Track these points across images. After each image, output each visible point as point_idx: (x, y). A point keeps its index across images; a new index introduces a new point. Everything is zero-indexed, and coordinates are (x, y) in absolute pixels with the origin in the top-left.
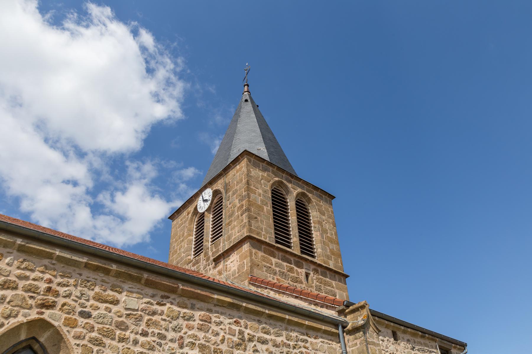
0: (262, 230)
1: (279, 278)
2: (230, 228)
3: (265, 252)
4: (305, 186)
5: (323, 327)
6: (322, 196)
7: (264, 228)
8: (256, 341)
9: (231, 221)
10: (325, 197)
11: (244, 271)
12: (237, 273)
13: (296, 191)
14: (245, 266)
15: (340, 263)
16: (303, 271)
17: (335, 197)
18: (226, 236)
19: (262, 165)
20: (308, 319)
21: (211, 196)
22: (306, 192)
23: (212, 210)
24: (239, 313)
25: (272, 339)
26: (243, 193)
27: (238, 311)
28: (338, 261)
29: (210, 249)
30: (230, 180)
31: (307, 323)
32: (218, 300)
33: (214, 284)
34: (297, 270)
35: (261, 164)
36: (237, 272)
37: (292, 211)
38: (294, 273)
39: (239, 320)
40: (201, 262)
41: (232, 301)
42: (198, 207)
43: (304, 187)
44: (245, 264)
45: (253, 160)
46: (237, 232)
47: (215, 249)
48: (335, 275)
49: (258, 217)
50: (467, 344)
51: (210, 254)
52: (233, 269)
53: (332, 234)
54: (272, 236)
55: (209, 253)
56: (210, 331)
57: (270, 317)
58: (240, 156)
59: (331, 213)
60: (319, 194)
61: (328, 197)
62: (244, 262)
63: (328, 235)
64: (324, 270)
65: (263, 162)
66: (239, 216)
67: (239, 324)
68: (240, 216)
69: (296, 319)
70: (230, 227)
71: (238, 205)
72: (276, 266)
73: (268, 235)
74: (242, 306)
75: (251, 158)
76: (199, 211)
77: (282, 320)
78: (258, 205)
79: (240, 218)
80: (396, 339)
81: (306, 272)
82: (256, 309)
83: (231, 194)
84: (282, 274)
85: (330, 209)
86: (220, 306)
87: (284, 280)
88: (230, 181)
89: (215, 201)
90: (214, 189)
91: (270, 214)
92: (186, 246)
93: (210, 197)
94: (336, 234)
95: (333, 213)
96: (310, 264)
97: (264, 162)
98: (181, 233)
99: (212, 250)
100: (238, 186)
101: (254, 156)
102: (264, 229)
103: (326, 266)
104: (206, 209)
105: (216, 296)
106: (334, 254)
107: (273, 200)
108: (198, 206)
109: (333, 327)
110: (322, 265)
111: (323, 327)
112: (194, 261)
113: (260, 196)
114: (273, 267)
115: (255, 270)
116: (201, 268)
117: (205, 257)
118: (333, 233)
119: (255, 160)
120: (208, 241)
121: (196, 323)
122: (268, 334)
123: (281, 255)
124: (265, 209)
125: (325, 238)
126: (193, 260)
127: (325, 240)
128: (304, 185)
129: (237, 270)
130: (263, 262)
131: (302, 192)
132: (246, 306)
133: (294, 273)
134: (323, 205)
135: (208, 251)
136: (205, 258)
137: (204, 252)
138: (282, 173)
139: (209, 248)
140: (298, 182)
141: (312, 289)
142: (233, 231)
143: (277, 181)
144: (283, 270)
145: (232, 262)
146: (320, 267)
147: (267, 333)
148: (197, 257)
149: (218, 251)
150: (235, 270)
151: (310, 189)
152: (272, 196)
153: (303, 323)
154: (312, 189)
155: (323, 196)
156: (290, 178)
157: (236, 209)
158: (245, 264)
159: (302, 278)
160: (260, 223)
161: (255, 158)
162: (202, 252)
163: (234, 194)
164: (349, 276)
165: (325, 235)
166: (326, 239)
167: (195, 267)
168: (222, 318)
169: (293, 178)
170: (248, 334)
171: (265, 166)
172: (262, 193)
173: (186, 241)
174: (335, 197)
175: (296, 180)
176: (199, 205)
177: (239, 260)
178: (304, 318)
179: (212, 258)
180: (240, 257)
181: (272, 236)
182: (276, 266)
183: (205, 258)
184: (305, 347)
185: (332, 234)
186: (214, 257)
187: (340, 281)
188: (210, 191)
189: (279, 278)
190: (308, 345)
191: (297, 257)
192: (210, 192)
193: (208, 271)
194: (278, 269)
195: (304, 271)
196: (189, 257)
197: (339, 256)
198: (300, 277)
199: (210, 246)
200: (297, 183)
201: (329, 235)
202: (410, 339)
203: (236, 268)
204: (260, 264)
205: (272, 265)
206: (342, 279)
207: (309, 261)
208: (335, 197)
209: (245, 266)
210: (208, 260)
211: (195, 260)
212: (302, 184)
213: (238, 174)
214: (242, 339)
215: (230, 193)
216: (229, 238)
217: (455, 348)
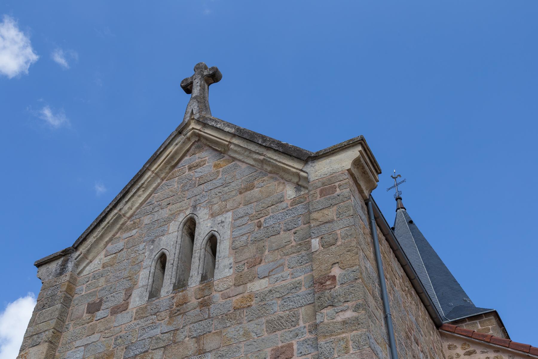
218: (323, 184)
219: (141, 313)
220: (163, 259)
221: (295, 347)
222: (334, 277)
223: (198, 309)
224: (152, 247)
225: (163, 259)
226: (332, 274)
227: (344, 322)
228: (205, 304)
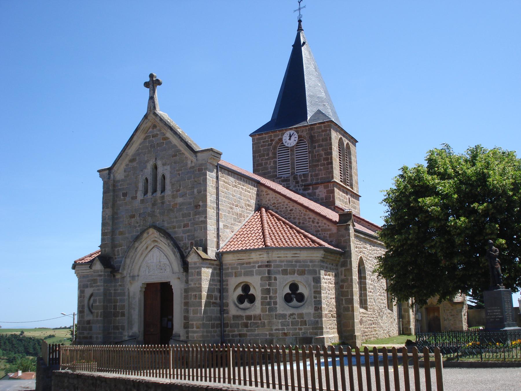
14: (332, 198)
17: (358, 142)
30: (316, 135)
65: (336, 126)
70: (317, 168)
90: (299, 134)
142: (320, 172)
149: (306, 180)
203: (324, 196)
209: (332, 198)
218: (199, 166)
219: (142, 201)
220: (147, 179)
221: (189, 224)
222: (200, 205)
223: (161, 204)
224: (142, 173)
225: (147, 179)
226: (199, 204)
227: (201, 221)
228: (163, 203)
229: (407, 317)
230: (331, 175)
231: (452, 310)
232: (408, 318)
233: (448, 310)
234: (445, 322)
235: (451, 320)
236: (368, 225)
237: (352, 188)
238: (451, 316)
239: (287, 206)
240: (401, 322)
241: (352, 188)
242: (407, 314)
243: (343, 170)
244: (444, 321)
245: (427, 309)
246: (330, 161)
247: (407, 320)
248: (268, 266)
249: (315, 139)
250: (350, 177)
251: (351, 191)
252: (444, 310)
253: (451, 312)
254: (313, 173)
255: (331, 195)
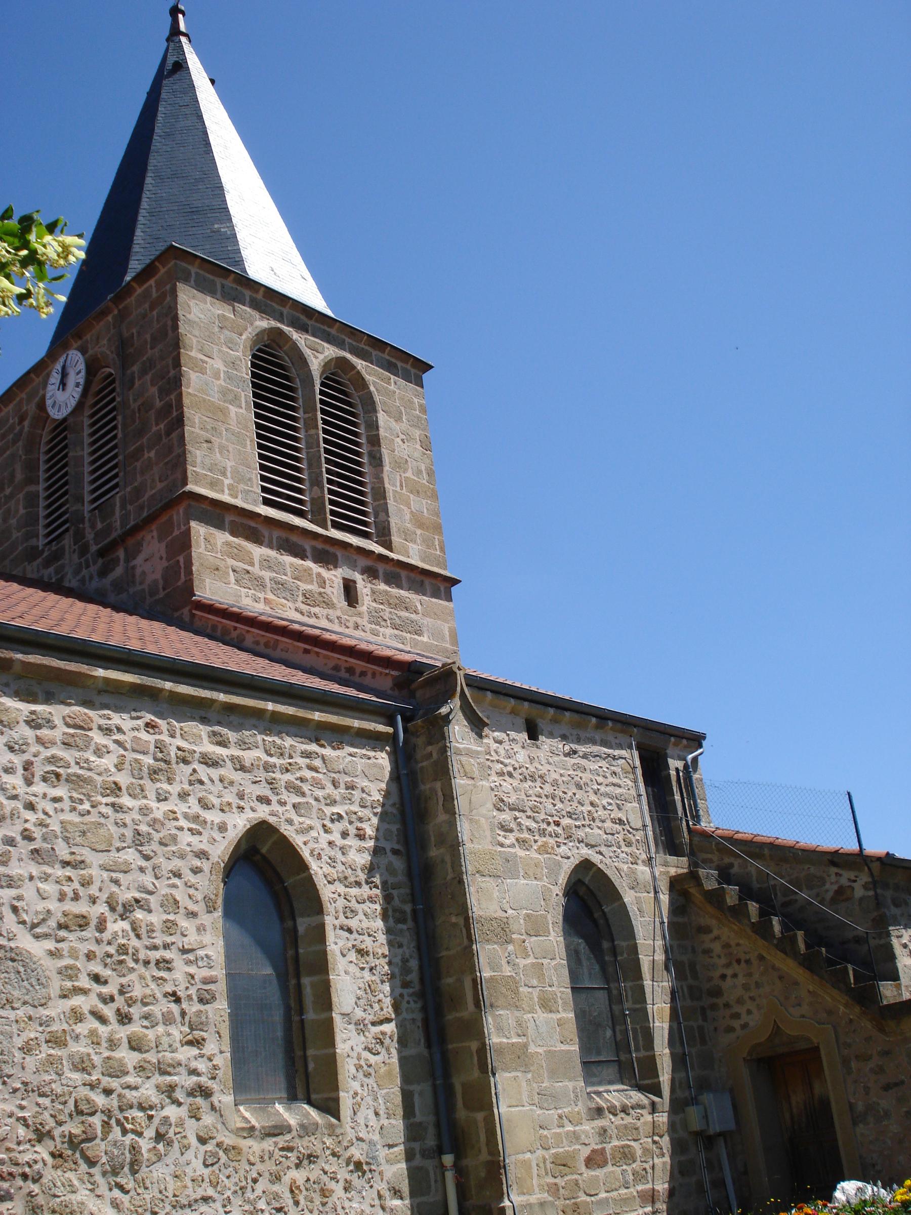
0: (224, 474)
1: (271, 596)
2: (138, 468)
3: (233, 534)
4: (347, 340)
5: (356, 724)
6: (395, 366)
7: (231, 467)
8: (196, 762)
9: (140, 450)
10: (405, 365)
11: (179, 583)
12: (161, 590)
13: (321, 357)
15: (437, 547)
16: (335, 576)
17: (432, 367)
18: (128, 489)
19: (223, 286)
20: (320, 707)
21: (83, 373)
22: (348, 356)
23: (88, 412)
24: (157, 706)
25: (233, 756)
26: (169, 372)
27: (154, 701)
28: (433, 544)
29: (87, 524)
30: (134, 331)
31: (317, 716)
32: (107, 680)
33: (95, 646)
34: (319, 575)
35: (218, 281)
36: (161, 587)
37: (310, 415)
38: (313, 581)
39: (156, 720)
40: (67, 556)
41: (139, 682)
42: (49, 402)
43: (344, 341)
44: (182, 566)
45: (197, 274)
46: (157, 479)
47: (102, 522)
48: (422, 582)
49: (213, 439)
50: (707, 736)
51: (90, 535)
52: (149, 579)
53: (419, 472)
54: (251, 489)
55: (87, 535)
56: (92, 747)
57: (230, 708)
58: (159, 262)
59: (418, 412)
60: (387, 360)
61: (413, 366)
62: (178, 561)
63: (406, 475)
64: (393, 569)
65: (226, 277)
66: (161, 435)
67: (157, 730)
68: (164, 437)
69: (290, 710)
71: (158, 404)
72: (262, 567)
73: (242, 486)
74: (161, 690)
75: (190, 267)
76: (51, 413)
77: (259, 714)
78: (213, 403)
79: (164, 440)
80: (533, 735)
81: (344, 579)
82: (196, 694)
83: (136, 372)
84: (279, 587)
85: (416, 400)
86: (113, 693)
87: (286, 602)
88: (133, 334)
89: (95, 388)
91: (246, 428)
92: (22, 511)
93: (80, 375)
94: (430, 473)
95: (423, 409)
96: (355, 557)
97: (228, 276)
98: (5, 474)
99: (93, 526)
100: (156, 350)
101: (198, 261)
102: (229, 469)
103: (398, 561)
104: (70, 409)
105: (100, 672)
106: (424, 524)
107: (254, 385)
108: (47, 401)
109: (382, 720)
110: (388, 557)
111: (356, 724)
112: (46, 554)
113: (218, 379)
114: (256, 570)
115: (207, 580)
116: (67, 573)
117: (74, 545)
118: (423, 468)
119: (202, 272)
120: (80, 499)
121: (60, 731)
122: (225, 746)
123: (277, 538)
124: (233, 415)
125: (398, 484)
126: (43, 551)
127: (398, 489)
128: (344, 337)
129: (161, 583)
130: (228, 559)
131: (337, 358)
132: (173, 690)
133: (311, 582)
134: (398, 391)
135: (84, 528)
136: (76, 547)
137: (71, 532)
138: (281, 306)
139: (87, 519)
140: (326, 328)
141: (359, 620)
143: (265, 330)
144: (284, 577)
145: (147, 559)
146: (382, 562)
147: (223, 744)
148: (54, 543)
149: (108, 529)
150: (155, 582)
151: (362, 346)
152: (254, 375)
153: (310, 716)
154: (367, 348)
155: (399, 364)
156: (302, 317)
157: (152, 415)
158: (182, 566)
159: (333, 593)
160: (218, 454)
161: (200, 267)
162: (67, 530)
163: (143, 372)
164: (461, 581)
165: (400, 476)
166: (401, 486)
167: (51, 570)
168: (116, 719)
169: (311, 319)
170: (179, 749)
171: (232, 287)
172: (222, 368)
173: (21, 496)
174: (432, 365)
175: (322, 324)
176: (51, 397)
177: (164, 556)
178: (310, 705)
179: (94, 548)
180: (167, 546)
181: (252, 487)
182: (262, 567)
183: (76, 547)
184: (311, 768)
185: (419, 472)
186: (99, 546)
187: (436, 594)
188: (77, 358)
189: (271, 596)
190: (317, 763)
191: (320, 539)
192: (79, 363)
193: (87, 582)
194: (267, 575)
195: (339, 576)
196: (33, 542)
197: (437, 528)
198: (328, 590)
199: (87, 515)
200: (324, 331)
201: (409, 474)
202: (568, 734)
203: (158, 576)
204: (221, 565)
205: (252, 564)
206: (442, 589)
207: (352, 550)
208: (432, 367)
209: (182, 571)
210: (84, 551)
211: (49, 550)
212: (338, 332)
213: (155, 313)
214: (166, 761)
215: (135, 368)
216: (138, 492)
217: (676, 744)
229: (483, 1138)
230: (179, 475)
231: (886, 1053)
232: (488, 1143)
233: (864, 1058)
234: (861, 1128)
235: (887, 1114)
236: (306, 651)
237: (389, 546)
238: (887, 1088)
239: (135, 1028)
240: (450, 1176)
241: (389, 546)
242: (480, 1116)
243: (310, 466)
244: (855, 1124)
245: (155, 1147)
246: (175, 414)
247: (484, 1156)
248: (345, 928)
249: (131, 350)
250: (375, 500)
251: (322, 536)
252: (846, 1061)
253: (880, 1070)
254: (128, 489)
255: (181, 559)
